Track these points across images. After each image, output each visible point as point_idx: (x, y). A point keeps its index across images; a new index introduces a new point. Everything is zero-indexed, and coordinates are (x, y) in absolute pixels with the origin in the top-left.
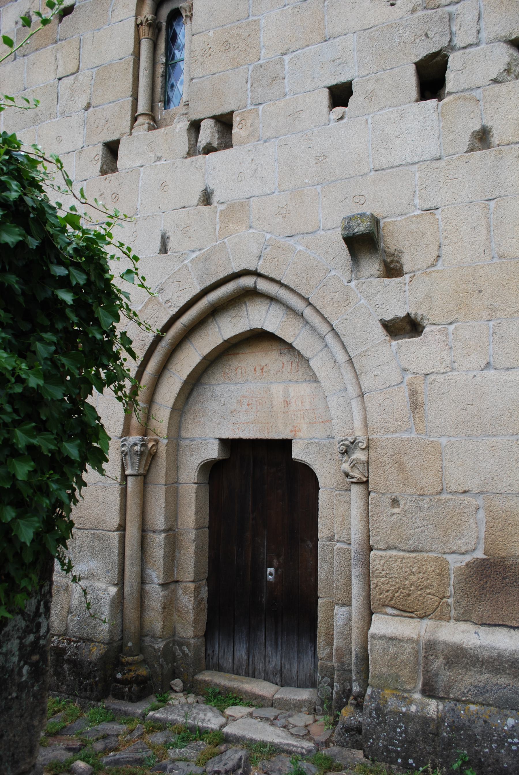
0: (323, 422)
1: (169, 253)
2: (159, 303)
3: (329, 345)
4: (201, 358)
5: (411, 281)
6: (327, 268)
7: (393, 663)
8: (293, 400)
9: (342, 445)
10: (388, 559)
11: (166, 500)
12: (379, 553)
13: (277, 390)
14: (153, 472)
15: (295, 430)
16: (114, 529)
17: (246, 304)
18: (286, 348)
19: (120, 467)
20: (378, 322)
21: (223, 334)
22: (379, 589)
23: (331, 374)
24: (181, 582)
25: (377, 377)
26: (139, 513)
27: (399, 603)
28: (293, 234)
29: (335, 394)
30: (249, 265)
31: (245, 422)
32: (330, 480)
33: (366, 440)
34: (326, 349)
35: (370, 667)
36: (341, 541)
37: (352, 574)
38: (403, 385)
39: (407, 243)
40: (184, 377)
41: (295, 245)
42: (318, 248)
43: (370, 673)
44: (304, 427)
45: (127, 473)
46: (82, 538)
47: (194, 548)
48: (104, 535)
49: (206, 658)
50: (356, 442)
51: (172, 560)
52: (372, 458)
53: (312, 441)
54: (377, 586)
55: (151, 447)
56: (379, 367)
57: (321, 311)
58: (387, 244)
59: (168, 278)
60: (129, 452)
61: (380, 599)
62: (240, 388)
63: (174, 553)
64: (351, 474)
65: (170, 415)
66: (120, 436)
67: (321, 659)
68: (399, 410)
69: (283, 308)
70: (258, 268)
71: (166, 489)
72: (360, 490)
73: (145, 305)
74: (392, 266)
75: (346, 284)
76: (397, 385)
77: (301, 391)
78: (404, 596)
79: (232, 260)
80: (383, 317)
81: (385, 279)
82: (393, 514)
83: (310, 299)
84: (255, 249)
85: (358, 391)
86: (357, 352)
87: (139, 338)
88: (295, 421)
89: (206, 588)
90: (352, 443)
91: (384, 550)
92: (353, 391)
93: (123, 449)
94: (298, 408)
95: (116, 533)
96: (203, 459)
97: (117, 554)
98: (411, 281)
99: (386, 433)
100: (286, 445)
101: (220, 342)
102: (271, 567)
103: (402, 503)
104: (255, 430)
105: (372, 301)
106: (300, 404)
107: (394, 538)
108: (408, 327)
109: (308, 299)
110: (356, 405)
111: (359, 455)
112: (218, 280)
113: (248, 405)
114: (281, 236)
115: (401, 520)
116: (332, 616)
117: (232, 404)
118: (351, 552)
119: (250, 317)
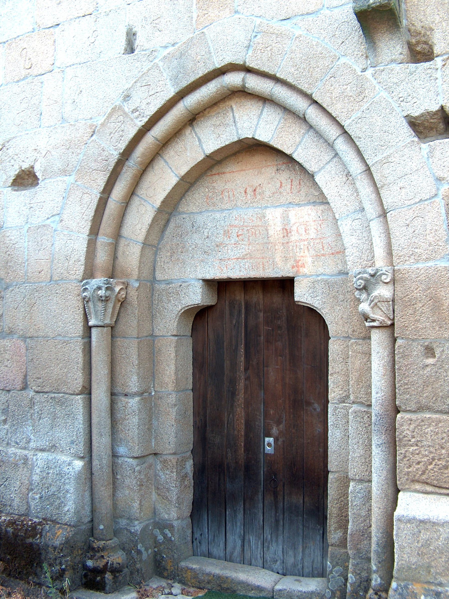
0: (333, 254)
1: (136, 52)
2: (125, 113)
3: (340, 153)
4: (178, 179)
5: (444, 65)
6: (335, 55)
7: (425, 551)
8: (294, 228)
9: (359, 279)
10: (420, 422)
11: (139, 356)
12: (408, 416)
13: (274, 216)
14: (122, 321)
15: (297, 265)
16: (77, 392)
17: (232, 109)
18: (284, 163)
19: (82, 316)
20: (403, 119)
21: (204, 147)
22: (408, 460)
23: (342, 191)
24: (160, 454)
25: (403, 190)
26: (106, 372)
27: (433, 478)
28: (290, 16)
29: (348, 215)
30: (234, 58)
31: (235, 257)
32: (343, 326)
33: (391, 271)
34: (335, 160)
35: (396, 556)
36: (358, 403)
37: (373, 442)
38: (438, 200)
39: (437, 18)
40: (158, 204)
41: (292, 30)
42: (322, 31)
43: (395, 564)
44: (309, 260)
45: (91, 323)
46: (41, 402)
47: (175, 414)
48: (66, 399)
49: (193, 542)
50: (378, 274)
51: (148, 429)
52: (399, 294)
53: (319, 278)
54: (405, 457)
55: (119, 293)
56: (406, 177)
57: (328, 109)
58: (411, 20)
59: (135, 82)
60: (91, 298)
61: (408, 473)
62: (227, 215)
63: (150, 420)
64: (372, 315)
65: (142, 251)
66: (80, 278)
67: (332, 545)
68: (433, 231)
69: (279, 111)
70: (247, 61)
71: (139, 343)
72: (384, 336)
73: (107, 117)
74: (418, 49)
75: (360, 74)
76: (430, 199)
77: (306, 216)
78: (439, 469)
79: (213, 54)
80: (409, 112)
81: (410, 65)
82: (427, 366)
83: (313, 95)
84: (241, 37)
85: (379, 209)
86: (376, 159)
87: (101, 158)
88: (298, 254)
89: (191, 462)
90: (373, 276)
91: (414, 411)
92: (372, 210)
93: (85, 294)
94: (301, 238)
95: (79, 396)
96: (183, 306)
97: (82, 422)
98: (444, 65)
99: (417, 261)
100: (286, 285)
101: (201, 157)
102: (269, 436)
103: (438, 352)
104: (247, 267)
105: (394, 93)
106: (304, 233)
107: (427, 397)
108: (442, 126)
109: (311, 95)
110: (376, 227)
111: (383, 292)
112: (197, 80)
113: (238, 236)
114: (275, 20)
115: (436, 372)
116: (346, 495)
117: (218, 236)
118: (371, 415)
119: (238, 125)
